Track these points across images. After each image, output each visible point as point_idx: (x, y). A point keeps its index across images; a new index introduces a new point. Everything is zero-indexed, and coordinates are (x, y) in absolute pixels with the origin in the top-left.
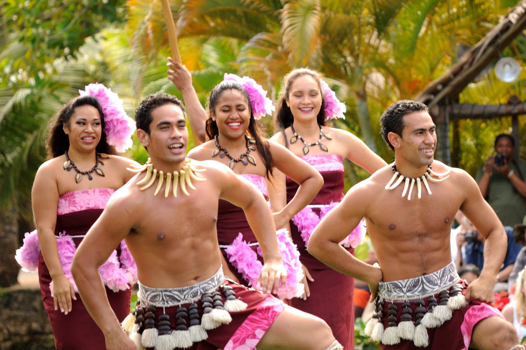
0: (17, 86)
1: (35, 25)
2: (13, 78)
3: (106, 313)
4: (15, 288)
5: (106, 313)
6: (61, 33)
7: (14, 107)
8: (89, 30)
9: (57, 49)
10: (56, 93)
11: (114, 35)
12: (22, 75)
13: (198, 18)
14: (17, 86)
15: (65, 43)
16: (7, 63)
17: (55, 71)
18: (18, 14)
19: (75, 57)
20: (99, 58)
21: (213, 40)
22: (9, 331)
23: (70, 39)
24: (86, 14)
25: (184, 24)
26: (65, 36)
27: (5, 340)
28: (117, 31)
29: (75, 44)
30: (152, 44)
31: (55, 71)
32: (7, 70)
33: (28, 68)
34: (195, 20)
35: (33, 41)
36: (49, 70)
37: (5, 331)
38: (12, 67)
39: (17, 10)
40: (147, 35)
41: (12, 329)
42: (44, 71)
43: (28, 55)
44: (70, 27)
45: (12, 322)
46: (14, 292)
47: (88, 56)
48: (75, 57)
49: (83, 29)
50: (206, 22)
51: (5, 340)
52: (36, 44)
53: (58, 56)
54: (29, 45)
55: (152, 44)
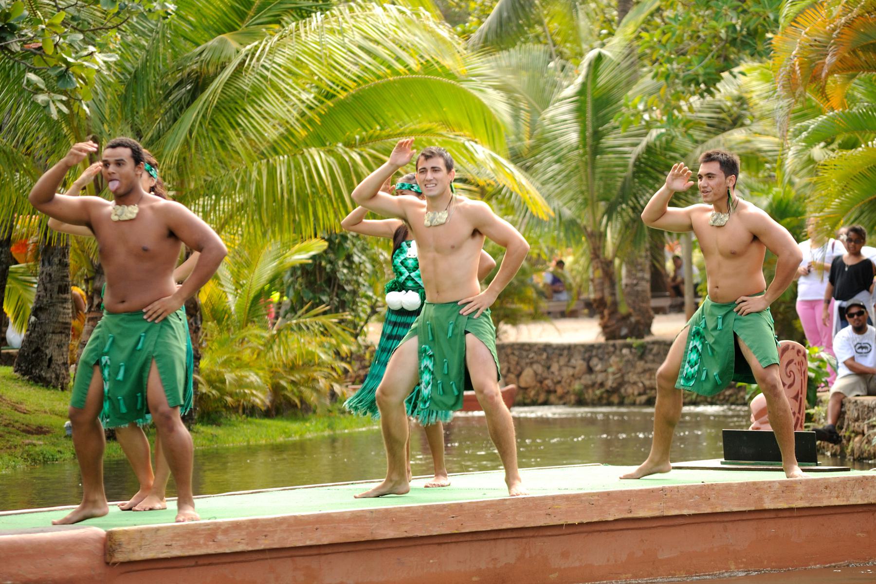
0: (649, 125)
1: (669, 61)
2: (646, 116)
3: (475, 36)
4: (648, 339)
5: (475, 36)
6: (697, 69)
7: (649, 149)
8: (728, 64)
9: (693, 87)
10: (691, 132)
11: (755, 69)
12: (657, 114)
13: (849, 53)
14: (649, 125)
15: (701, 79)
16: (641, 101)
17: (691, 109)
18: (652, 47)
19: (711, 94)
20: (735, 93)
21: (863, 75)
22: (644, 385)
23: (705, 74)
24: (724, 48)
25: (834, 59)
26: (701, 71)
27: (640, 394)
28: (756, 64)
29: (712, 80)
30: (799, 81)
31: (691, 109)
32: (641, 107)
33: (662, 106)
34: (847, 55)
35: (667, 77)
36: (685, 108)
37: (641, 385)
38: (646, 105)
39: (652, 44)
40: (794, 71)
41: (647, 383)
42: (679, 108)
43: (662, 92)
44: (706, 61)
45: (647, 375)
46: (648, 343)
47: (726, 89)
48: (711, 94)
49: (721, 63)
50: (858, 56)
51: (640, 394)
52: (670, 81)
53: (693, 94)
54: (663, 81)
55: (799, 81)
